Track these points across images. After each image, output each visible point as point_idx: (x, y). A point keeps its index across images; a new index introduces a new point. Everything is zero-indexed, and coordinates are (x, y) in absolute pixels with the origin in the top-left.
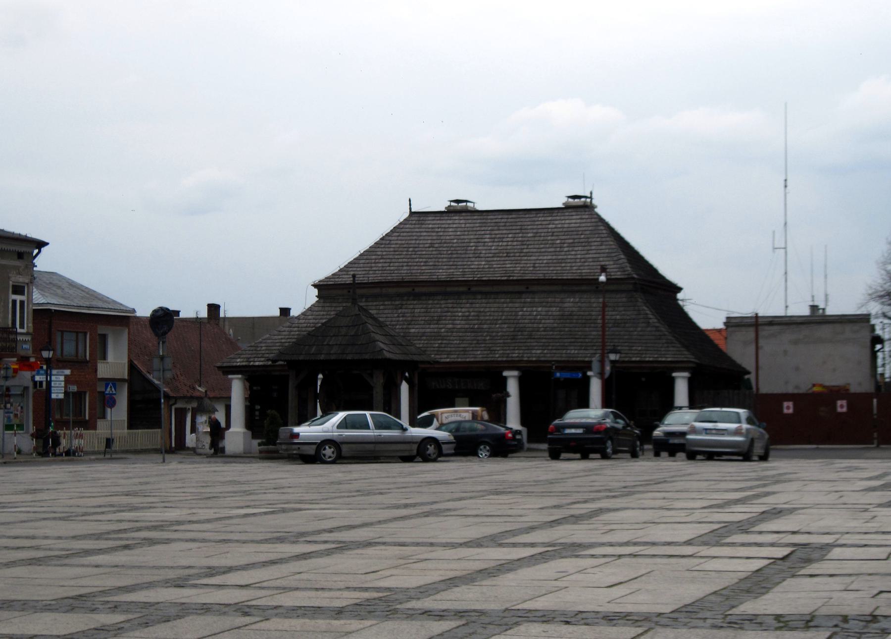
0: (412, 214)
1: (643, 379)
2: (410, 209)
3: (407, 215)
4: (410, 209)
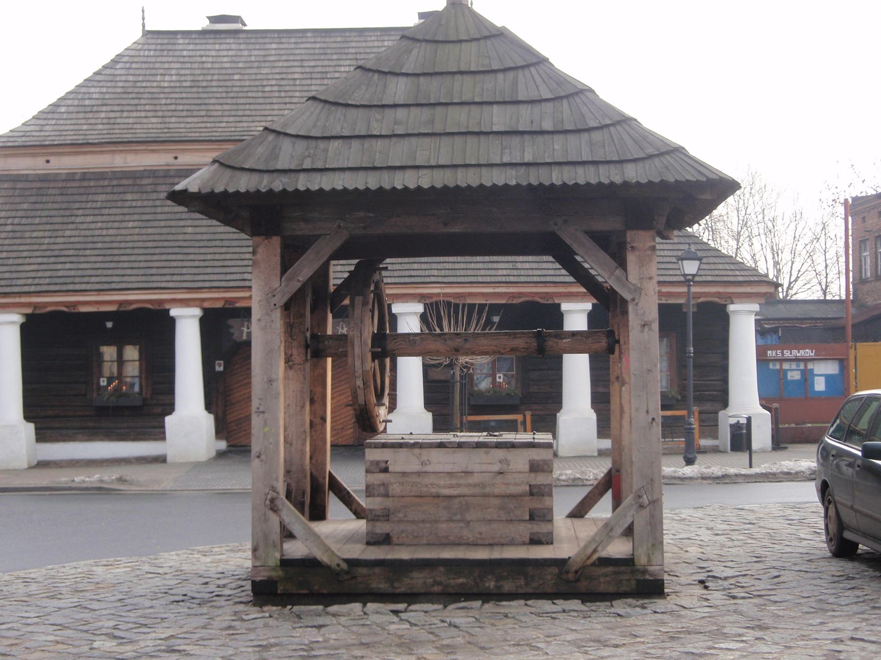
0: (147, 34)
1: (109, 325)
2: (144, 26)
3: (137, 35)
4: (144, 26)
